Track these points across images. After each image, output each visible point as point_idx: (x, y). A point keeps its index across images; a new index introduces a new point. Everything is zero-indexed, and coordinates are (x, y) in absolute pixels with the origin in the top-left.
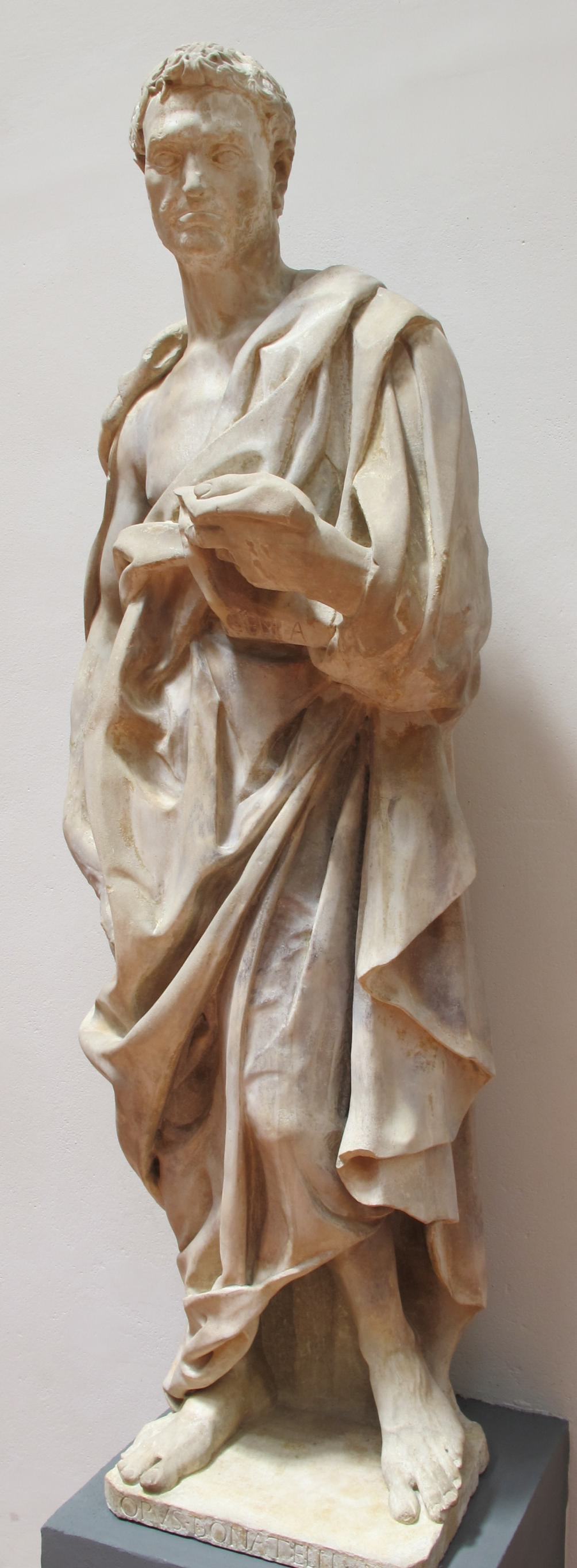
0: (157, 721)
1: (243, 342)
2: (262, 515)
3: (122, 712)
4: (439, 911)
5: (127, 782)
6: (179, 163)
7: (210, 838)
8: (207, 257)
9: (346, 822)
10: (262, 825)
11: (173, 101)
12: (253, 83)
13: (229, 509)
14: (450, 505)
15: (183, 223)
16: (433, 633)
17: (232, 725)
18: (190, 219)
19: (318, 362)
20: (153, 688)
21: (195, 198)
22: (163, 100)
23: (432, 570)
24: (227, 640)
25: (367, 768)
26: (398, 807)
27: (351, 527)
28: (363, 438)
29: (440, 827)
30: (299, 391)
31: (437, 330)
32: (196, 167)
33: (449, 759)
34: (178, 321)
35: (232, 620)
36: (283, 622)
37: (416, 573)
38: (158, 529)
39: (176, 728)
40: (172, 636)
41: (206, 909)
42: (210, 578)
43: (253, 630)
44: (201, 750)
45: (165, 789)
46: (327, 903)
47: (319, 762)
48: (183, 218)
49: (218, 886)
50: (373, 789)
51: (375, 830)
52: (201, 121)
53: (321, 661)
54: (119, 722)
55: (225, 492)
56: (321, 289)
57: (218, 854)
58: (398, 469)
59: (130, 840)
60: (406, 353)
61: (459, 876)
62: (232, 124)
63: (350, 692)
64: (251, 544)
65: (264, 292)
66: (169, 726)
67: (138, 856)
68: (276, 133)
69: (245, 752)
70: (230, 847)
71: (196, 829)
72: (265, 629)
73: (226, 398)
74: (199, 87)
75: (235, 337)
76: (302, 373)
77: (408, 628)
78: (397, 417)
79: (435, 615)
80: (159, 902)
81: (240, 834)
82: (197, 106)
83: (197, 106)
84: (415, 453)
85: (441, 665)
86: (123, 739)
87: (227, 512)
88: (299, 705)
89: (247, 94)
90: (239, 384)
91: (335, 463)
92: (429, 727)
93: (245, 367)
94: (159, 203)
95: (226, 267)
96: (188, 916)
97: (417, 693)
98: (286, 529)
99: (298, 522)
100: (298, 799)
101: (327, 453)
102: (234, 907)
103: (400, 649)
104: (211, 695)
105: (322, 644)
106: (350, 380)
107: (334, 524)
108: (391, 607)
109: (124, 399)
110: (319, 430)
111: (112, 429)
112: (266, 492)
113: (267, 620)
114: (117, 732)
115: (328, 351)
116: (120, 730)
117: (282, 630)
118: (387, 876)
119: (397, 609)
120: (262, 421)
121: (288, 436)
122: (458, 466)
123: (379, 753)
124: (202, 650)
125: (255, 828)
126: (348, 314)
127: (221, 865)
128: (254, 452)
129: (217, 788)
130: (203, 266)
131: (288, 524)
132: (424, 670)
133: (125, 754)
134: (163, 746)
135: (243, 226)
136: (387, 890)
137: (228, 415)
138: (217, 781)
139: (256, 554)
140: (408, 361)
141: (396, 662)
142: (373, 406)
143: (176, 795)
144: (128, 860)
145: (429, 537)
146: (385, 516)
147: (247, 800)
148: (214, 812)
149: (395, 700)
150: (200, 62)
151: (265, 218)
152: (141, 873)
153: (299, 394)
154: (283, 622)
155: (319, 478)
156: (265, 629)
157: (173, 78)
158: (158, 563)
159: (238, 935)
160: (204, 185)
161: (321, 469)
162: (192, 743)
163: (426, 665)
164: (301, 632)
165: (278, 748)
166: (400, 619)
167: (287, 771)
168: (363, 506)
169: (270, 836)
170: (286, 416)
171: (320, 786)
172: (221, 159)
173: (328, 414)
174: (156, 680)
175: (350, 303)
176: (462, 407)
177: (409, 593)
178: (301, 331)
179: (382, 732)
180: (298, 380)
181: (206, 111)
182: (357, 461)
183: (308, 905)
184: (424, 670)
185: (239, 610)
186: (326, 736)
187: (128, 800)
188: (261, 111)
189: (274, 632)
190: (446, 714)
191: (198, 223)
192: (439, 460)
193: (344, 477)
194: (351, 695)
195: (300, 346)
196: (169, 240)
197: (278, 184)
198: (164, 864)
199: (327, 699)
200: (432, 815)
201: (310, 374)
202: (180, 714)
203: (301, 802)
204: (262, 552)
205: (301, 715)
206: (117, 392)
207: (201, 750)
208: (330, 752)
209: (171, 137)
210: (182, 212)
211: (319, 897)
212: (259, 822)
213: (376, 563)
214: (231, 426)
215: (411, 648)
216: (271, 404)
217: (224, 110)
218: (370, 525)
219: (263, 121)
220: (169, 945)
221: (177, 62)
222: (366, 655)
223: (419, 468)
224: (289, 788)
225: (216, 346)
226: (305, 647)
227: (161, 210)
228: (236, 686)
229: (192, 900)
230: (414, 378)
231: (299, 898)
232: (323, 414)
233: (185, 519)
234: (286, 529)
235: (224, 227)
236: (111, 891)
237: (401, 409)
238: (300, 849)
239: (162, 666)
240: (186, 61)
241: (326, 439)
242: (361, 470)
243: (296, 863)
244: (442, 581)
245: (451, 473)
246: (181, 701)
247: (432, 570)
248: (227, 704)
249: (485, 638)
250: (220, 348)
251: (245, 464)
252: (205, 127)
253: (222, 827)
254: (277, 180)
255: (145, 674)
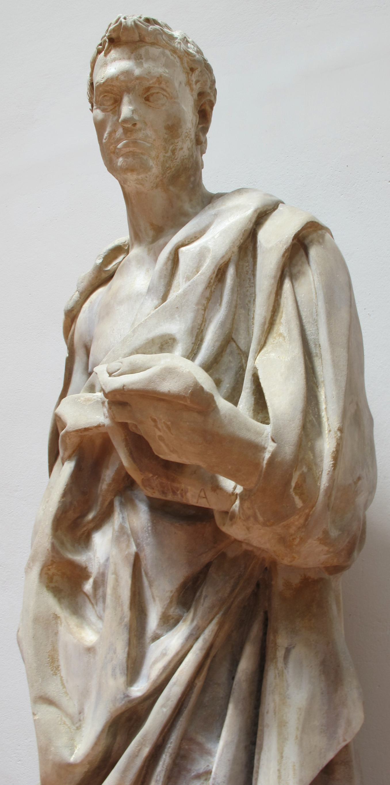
0: (84, 565)
1: (165, 244)
2: (163, 394)
3: (53, 557)
4: (331, 756)
5: (56, 617)
6: (117, 102)
7: (122, 680)
8: (140, 177)
9: (245, 665)
10: (168, 670)
11: (113, 54)
12: (179, 43)
13: (135, 387)
14: (343, 384)
15: (120, 149)
16: (327, 506)
17: (146, 574)
18: (126, 146)
19: (226, 259)
20: (83, 534)
21: (130, 127)
22: (106, 55)
23: (327, 445)
24: (145, 498)
25: (266, 613)
26: (294, 654)
27: (253, 402)
28: (265, 323)
29: (331, 674)
30: (210, 283)
31: (328, 235)
32: (130, 103)
33: (338, 603)
34: (122, 235)
35: (146, 483)
36: (189, 488)
37: (312, 449)
38: (88, 400)
39: (98, 573)
40: (99, 492)
41: (119, 739)
42: (127, 445)
43: (164, 493)
44: (117, 597)
45: (90, 624)
46: (226, 745)
47: (221, 613)
48: (120, 146)
49: (129, 719)
50: (271, 637)
51: (271, 677)
52: (135, 67)
53: (224, 525)
54: (52, 565)
55: (133, 371)
56: (230, 203)
57: (128, 696)
58: (294, 351)
59: (56, 669)
60: (302, 252)
61: (349, 723)
62: (159, 70)
63: (250, 548)
64: (154, 421)
65: (187, 207)
66: (94, 569)
67: (63, 685)
68: (199, 85)
69: (157, 599)
70: (139, 689)
71: (109, 671)
72: (174, 493)
73: (149, 290)
74: (134, 42)
75: (161, 241)
76: (213, 267)
77: (304, 501)
78: (295, 305)
79: (329, 489)
80: (78, 728)
81: (148, 677)
82: (133, 56)
83: (133, 56)
84: (311, 337)
85: (334, 533)
86: (55, 578)
87: (132, 390)
88: (205, 559)
89: (174, 51)
90: (160, 277)
91: (240, 345)
92: (321, 580)
93: (166, 264)
94: (103, 136)
95: (157, 187)
96: (101, 748)
97: (312, 554)
98: (187, 408)
99: (197, 402)
100: (201, 649)
101: (234, 337)
102: (140, 750)
103: (297, 521)
104: (128, 546)
105: (225, 509)
106: (254, 275)
107: (236, 404)
108: (288, 483)
109: (81, 294)
110: (227, 316)
111: (71, 316)
112: (168, 372)
113: (176, 485)
114: (50, 573)
115: (236, 249)
116: (53, 571)
117: (189, 495)
118: (282, 725)
119: (293, 484)
120: (177, 308)
121: (199, 322)
122: (349, 348)
123: (276, 603)
124: (123, 505)
125: (161, 674)
126: (253, 220)
127: (130, 705)
128: (169, 335)
129: (130, 632)
130: (138, 186)
131: (188, 403)
132: (319, 539)
133: (57, 592)
134: (88, 587)
135: (169, 154)
136: (282, 739)
137: (150, 304)
138: (131, 626)
139: (159, 430)
140: (304, 259)
141: (292, 531)
142: (273, 296)
143: (95, 632)
144: (53, 689)
145: (323, 414)
146: (283, 394)
147: (158, 642)
148: (125, 655)
149: (291, 562)
150: (134, 22)
151: (189, 149)
152: (64, 701)
153: (209, 286)
154: (189, 488)
155: (227, 358)
156: (174, 493)
157: (114, 36)
158: (86, 429)
159: (144, 772)
160: (136, 117)
161: (228, 350)
162: (109, 590)
163: (320, 535)
164: (206, 497)
165: (187, 596)
166: (296, 494)
167: (193, 620)
168: (263, 385)
169: (175, 684)
170: (197, 304)
171: (222, 634)
172: (151, 99)
173: (234, 303)
174: (85, 529)
175: (255, 211)
176: (351, 302)
177: (305, 469)
178: (215, 234)
179: (279, 583)
180: (209, 273)
181: (139, 59)
182: (259, 344)
183: (209, 746)
184: (319, 539)
185: (151, 475)
186: (228, 590)
187: (56, 634)
188: (186, 65)
189: (182, 496)
190: (336, 569)
191: (131, 149)
192: (332, 343)
193: (247, 357)
194: (252, 552)
195: (211, 245)
196: (112, 167)
197: (200, 126)
198: (84, 694)
199: (231, 554)
200: (323, 663)
201: (219, 269)
202: (102, 561)
203: (204, 652)
204: (165, 428)
205: (208, 566)
206: (76, 289)
207: (117, 597)
208: (232, 603)
209: (111, 81)
210: (119, 141)
211: (219, 736)
212: (165, 668)
213: (273, 440)
214: (153, 312)
215: (306, 520)
216: (185, 294)
217: (155, 59)
218: (268, 404)
219: (188, 73)
220: (86, 770)
221: (117, 22)
222: (264, 524)
223: (314, 350)
224: (193, 637)
225: (146, 249)
226: (212, 509)
227: (104, 141)
228: (150, 540)
229: (105, 735)
230: (310, 272)
231: (200, 739)
232: (230, 303)
233: (99, 395)
234: (187, 408)
235: (153, 153)
236: (37, 717)
237: (298, 299)
238: (204, 690)
239: (90, 516)
240: (123, 20)
241: (233, 324)
242: (263, 351)
243: (199, 708)
244: (336, 457)
245: (343, 354)
246: (103, 550)
247: (327, 445)
248: (142, 555)
249: (371, 501)
250: (149, 250)
251: (162, 345)
252: (137, 72)
253: (133, 668)
254: (199, 124)
255: (75, 521)
